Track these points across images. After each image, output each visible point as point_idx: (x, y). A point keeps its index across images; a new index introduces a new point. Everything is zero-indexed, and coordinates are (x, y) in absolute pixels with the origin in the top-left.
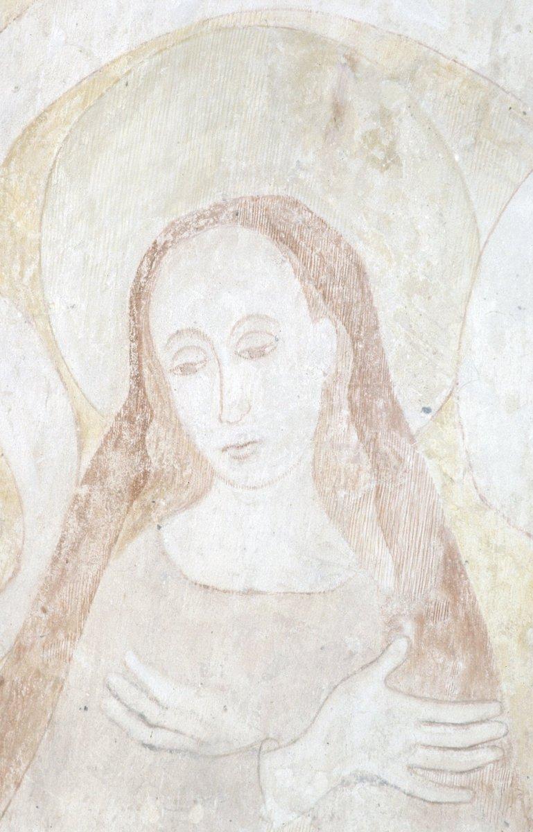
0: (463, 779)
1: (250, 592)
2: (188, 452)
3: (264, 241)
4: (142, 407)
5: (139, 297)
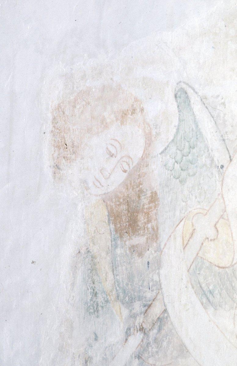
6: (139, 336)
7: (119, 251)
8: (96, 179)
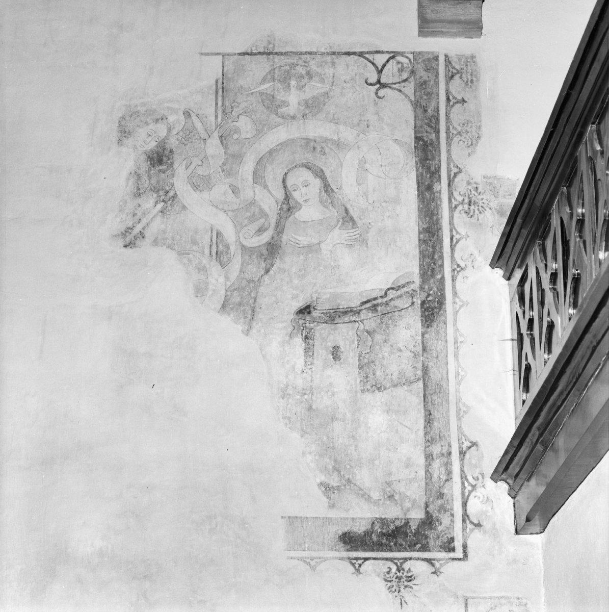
0: (355, 240)
1: (312, 221)
2: (297, 202)
3: (305, 169)
4: (287, 197)
5: (284, 181)
6: (162, 204)
7: (152, 172)
8: (423, 343)
